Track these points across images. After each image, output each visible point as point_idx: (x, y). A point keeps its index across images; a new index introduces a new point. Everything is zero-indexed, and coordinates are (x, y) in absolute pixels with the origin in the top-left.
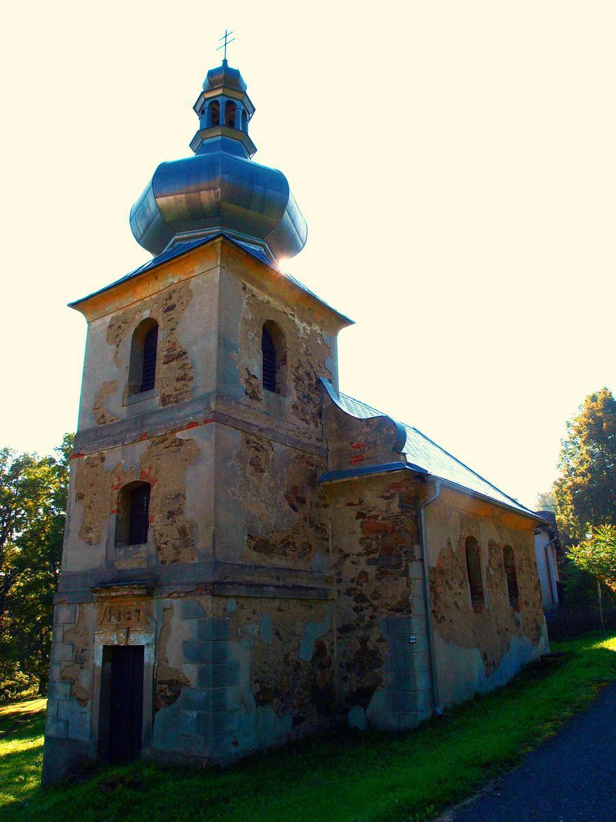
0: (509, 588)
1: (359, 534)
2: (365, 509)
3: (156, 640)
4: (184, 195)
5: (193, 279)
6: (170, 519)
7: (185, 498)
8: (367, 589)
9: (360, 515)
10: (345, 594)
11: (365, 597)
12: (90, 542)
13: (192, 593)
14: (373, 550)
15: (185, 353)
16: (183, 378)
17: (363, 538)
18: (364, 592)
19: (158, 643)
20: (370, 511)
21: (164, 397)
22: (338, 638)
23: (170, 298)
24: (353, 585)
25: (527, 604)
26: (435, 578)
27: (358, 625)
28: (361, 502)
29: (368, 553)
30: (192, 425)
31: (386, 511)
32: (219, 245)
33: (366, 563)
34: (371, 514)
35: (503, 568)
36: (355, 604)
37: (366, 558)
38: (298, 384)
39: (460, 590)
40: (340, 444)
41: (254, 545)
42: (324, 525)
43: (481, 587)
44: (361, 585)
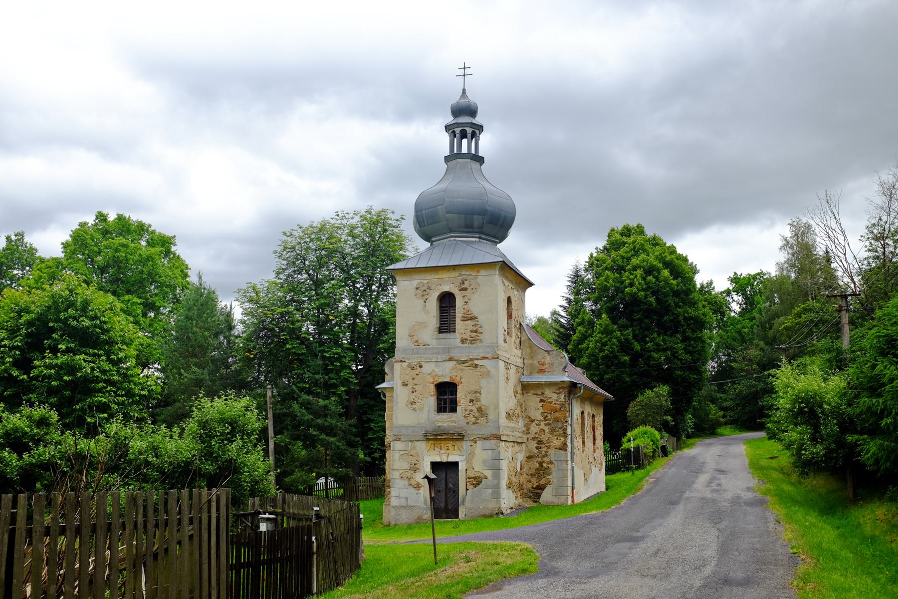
1: (541, 410)
7: (481, 394)
8: (544, 438)
9: (542, 401)
12: (414, 409)
16: (476, 331)
19: (468, 460)
22: (526, 461)
23: (464, 283)
24: (536, 436)
28: (543, 394)
29: (545, 420)
30: (484, 358)
31: (557, 400)
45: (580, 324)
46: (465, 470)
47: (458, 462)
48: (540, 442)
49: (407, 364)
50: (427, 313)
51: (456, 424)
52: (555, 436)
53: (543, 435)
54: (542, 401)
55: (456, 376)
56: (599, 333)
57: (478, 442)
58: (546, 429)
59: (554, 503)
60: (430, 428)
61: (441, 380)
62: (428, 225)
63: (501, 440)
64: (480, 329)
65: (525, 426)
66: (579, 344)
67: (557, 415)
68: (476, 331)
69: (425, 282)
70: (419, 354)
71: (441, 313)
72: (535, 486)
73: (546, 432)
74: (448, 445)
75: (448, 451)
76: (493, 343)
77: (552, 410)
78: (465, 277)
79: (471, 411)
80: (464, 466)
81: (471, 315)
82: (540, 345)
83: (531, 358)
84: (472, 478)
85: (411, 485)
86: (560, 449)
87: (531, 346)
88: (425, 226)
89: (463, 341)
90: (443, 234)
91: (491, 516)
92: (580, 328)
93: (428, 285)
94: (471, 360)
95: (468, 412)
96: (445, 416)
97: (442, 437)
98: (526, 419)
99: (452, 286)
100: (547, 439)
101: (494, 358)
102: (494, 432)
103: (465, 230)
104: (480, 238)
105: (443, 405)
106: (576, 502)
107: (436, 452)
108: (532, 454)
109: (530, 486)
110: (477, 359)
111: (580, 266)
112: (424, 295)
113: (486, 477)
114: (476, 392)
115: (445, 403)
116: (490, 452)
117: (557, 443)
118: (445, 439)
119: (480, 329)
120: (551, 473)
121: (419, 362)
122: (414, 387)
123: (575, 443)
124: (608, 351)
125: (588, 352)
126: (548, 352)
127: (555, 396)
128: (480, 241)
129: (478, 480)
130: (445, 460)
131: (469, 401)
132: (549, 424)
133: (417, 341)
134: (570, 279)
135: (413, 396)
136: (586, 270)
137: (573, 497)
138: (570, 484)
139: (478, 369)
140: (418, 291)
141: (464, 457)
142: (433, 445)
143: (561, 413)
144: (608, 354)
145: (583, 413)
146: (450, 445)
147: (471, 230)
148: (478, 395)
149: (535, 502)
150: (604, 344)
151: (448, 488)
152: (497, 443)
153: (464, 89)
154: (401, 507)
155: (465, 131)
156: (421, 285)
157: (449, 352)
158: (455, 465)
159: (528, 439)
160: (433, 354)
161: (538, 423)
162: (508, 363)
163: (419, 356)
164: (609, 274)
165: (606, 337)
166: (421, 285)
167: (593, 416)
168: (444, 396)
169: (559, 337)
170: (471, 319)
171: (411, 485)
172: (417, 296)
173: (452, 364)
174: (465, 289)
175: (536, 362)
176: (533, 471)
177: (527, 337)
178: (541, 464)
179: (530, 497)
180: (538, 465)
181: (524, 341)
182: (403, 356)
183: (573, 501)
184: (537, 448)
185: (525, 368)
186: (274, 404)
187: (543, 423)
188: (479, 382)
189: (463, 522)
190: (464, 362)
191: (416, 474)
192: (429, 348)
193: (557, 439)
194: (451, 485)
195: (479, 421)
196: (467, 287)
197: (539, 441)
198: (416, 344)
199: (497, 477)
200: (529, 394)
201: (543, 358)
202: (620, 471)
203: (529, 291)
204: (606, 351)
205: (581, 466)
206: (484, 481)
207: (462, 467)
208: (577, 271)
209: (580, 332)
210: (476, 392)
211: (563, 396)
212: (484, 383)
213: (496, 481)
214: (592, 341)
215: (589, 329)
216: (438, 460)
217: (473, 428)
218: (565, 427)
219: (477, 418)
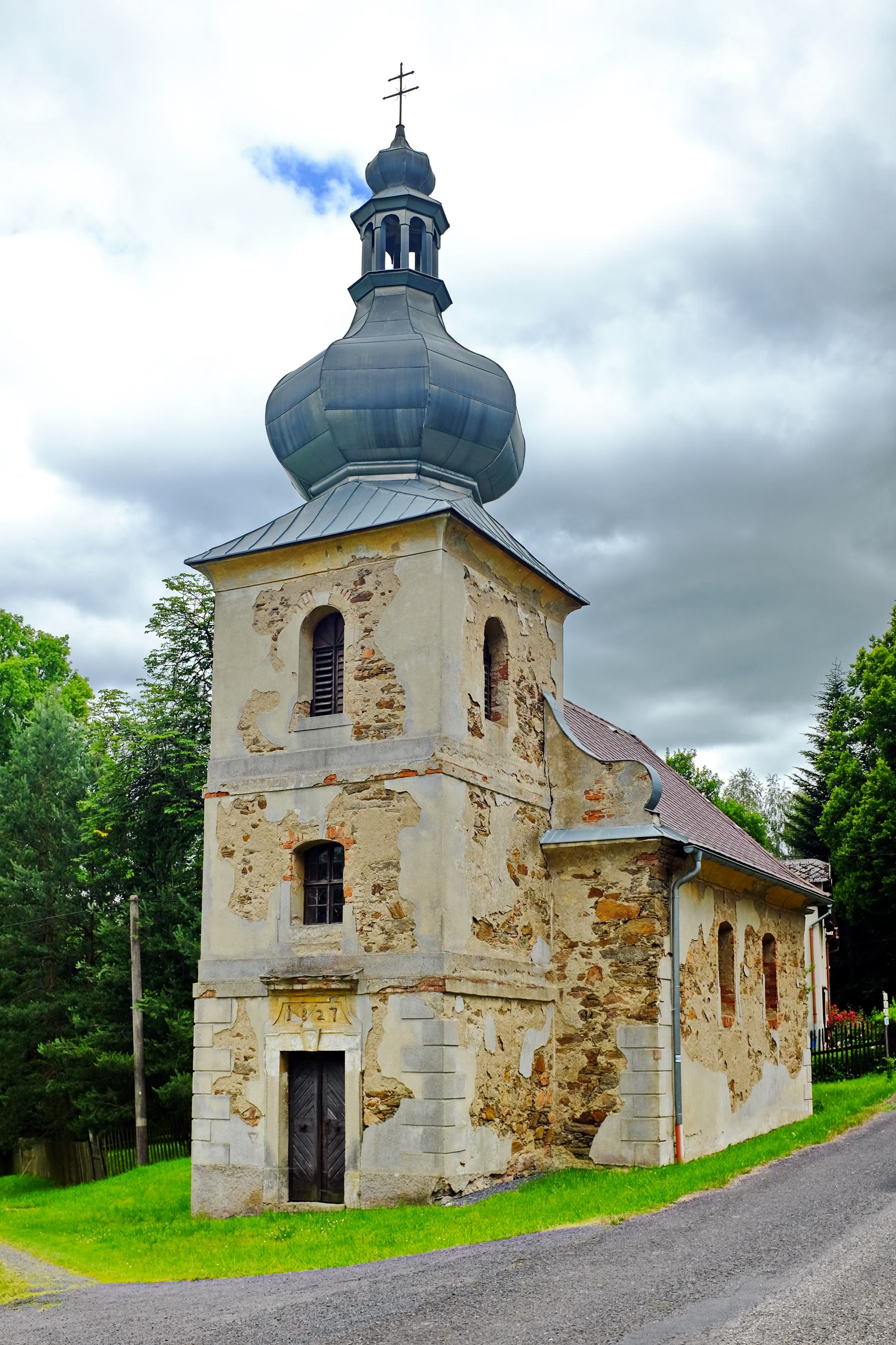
0: (767, 995)
1: (593, 918)
2: (601, 885)
3: (362, 1045)
4: (368, 411)
5: (399, 560)
6: (377, 894)
7: (399, 870)
8: (601, 991)
9: (594, 892)
10: (568, 994)
11: (597, 1000)
12: (247, 915)
13: (414, 989)
14: (610, 939)
15: (390, 669)
16: (390, 705)
17: (597, 923)
18: (596, 993)
19: (366, 1048)
20: (608, 888)
21: (359, 728)
22: (558, 1051)
23: (363, 582)
24: (582, 984)
25: (787, 1019)
26: (684, 979)
27: (586, 1035)
28: (597, 874)
29: (603, 943)
30: (407, 773)
31: (631, 890)
32: (446, 521)
33: (600, 956)
34: (611, 891)
35: (761, 965)
36: (583, 1008)
37: (600, 949)
38: (520, 706)
39: (710, 995)
40: (570, 792)
41: (477, 930)
42: (546, 902)
43: (733, 993)
44: (593, 984)
45: (837, 782)
46: (358, 1074)
47: (343, 1052)
48: (591, 1000)
49: (232, 799)
50: (278, 666)
51: (339, 953)
52: (628, 982)
53: (597, 983)
54: (594, 892)
55: (342, 825)
56: (871, 795)
57: (391, 998)
58: (605, 965)
59: (625, 1160)
60: (280, 966)
61: (307, 838)
62: (295, 450)
63: (445, 993)
64: (399, 697)
65: (554, 958)
66: (834, 820)
67: (633, 927)
68: (390, 705)
69: (276, 587)
70: (260, 774)
71: (316, 666)
72: (578, 1115)
73: (604, 973)
74: (320, 1007)
75: (321, 1024)
76: (429, 733)
77: (618, 916)
78: (365, 565)
79: (377, 915)
80: (358, 1062)
81: (380, 663)
82: (589, 745)
83: (569, 782)
84: (377, 1095)
85: (237, 1112)
86: (639, 1018)
87: (569, 751)
88: (289, 455)
89: (360, 732)
90: (330, 472)
91: (419, 1201)
92: (837, 789)
93: (281, 594)
94: (378, 779)
95: (369, 919)
96: (317, 931)
97: (305, 987)
98: (558, 941)
99: (336, 591)
100: (607, 991)
101: (429, 772)
102: (432, 971)
103: (379, 452)
104: (419, 472)
105: (317, 905)
106: (685, 1158)
107: (293, 1027)
108: (570, 1031)
109: (566, 1116)
110: (390, 777)
111: (843, 677)
112: (272, 622)
113: (409, 1095)
114: (387, 865)
115: (323, 899)
116: (418, 1025)
117: (633, 1002)
118: (314, 992)
119: (399, 697)
120: (617, 1082)
121: (259, 794)
122: (248, 857)
123: (693, 1002)
124: (889, 829)
125: (851, 834)
126: (609, 765)
127: (626, 880)
128: (419, 480)
129: (390, 1102)
130: (312, 1048)
131: (370, 889)
132: (612, 953)
133: (256, 741)
134: (823, 702)
135: (245, 882)
136: (853, 683)
137: (677, 1145)
138: (666, 1107)
139: (394, 802)
140: (262, 613)
141: (358, 1039)
142: (286, 1007)
143: (640, 923)
144: (888, 836)
145: (725, 930)
146: (324, 1007)
147: (394, 451)
148: (393, 872)
149: (579, 1156)
150: (881, 817)
151: (325, 1119)
152: (435, 1000)
153: (400, 128)
154: (215, 1168)
155: (396, 218)
156: (267, 596)
157: (326, 764)
158: (338, 1058)
159: (561, 993)
160: (290, 769)
161: (585, 949)
162: (483, 790)
163: (259, 777)
164: (890, 681)
165: (885, 803)
166: (267, 596)
167: (768, 941)
168: (320, 879)
169: (803, 811)
170: (381, 671)
171: (237, 1112)
172: (259, 625)
173: (333, 792)
174: (366, 597)
175: (579, 793)
176: (574, 1077)
177: (557, 731)
178: (592, 1056)
179: (567, 1143)
180: (584, 1061)
181: (552, 740)
182: (224, 781)
183: (677, 1156)
184: (584, 1015)
185: (553, 810)
186: (142, 932)
187: (596, 951)
188: (396, 838)
189: (360, 1214)
190: (361, 787)
191: (249, 1083)
192: (281, 756)
193: (632, 991)
194: (331, 1115)
195: (394, 942)
196: (371, 589)
197: (588, 998)
198: (254, 747)
199: (435, 1094)
200: (563, 877)
201: (597, 782)
202: (872, 1070)
203: (574, 617)
204: (884, 830)
205: (721, 1061)
206: (404, 1102)
207: (352, 1065)
208: (837, 686)
209: (836, 797)
210: (387, 865)
211: (645, 878)
212: (405, 839)
213: (433, 1105)
214: (858, 813)
215: (855, 790)
216: (299, 1048)
217: (378, 960)
218: (651, 959)
219: (389, 935)
